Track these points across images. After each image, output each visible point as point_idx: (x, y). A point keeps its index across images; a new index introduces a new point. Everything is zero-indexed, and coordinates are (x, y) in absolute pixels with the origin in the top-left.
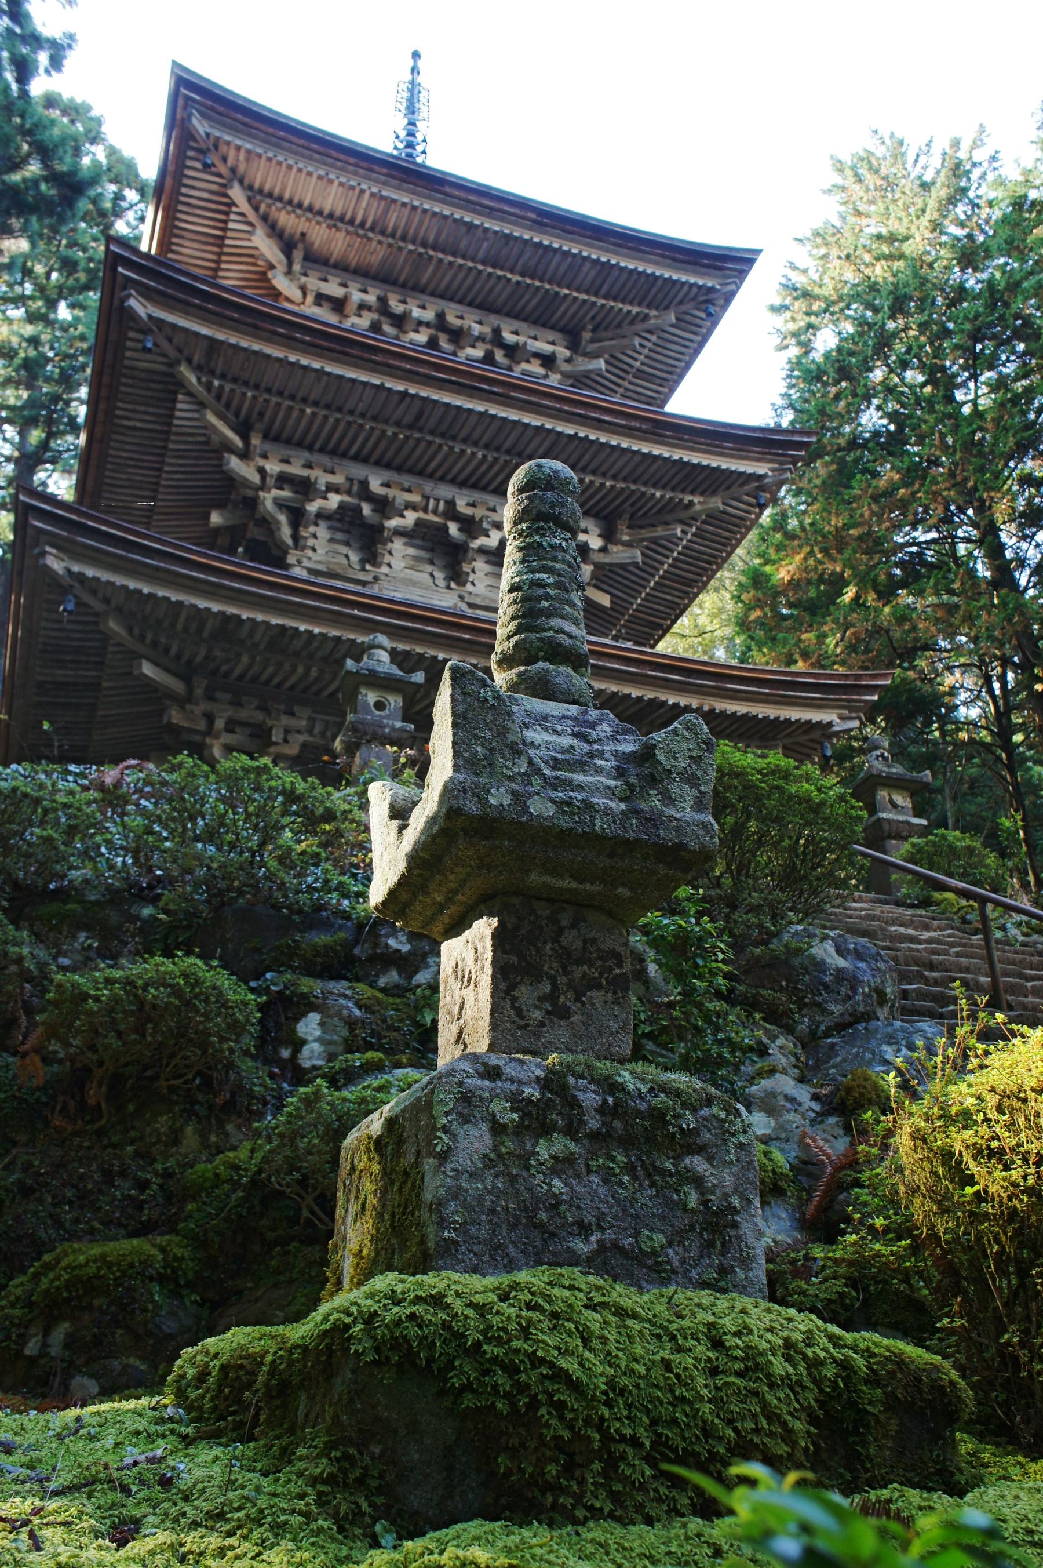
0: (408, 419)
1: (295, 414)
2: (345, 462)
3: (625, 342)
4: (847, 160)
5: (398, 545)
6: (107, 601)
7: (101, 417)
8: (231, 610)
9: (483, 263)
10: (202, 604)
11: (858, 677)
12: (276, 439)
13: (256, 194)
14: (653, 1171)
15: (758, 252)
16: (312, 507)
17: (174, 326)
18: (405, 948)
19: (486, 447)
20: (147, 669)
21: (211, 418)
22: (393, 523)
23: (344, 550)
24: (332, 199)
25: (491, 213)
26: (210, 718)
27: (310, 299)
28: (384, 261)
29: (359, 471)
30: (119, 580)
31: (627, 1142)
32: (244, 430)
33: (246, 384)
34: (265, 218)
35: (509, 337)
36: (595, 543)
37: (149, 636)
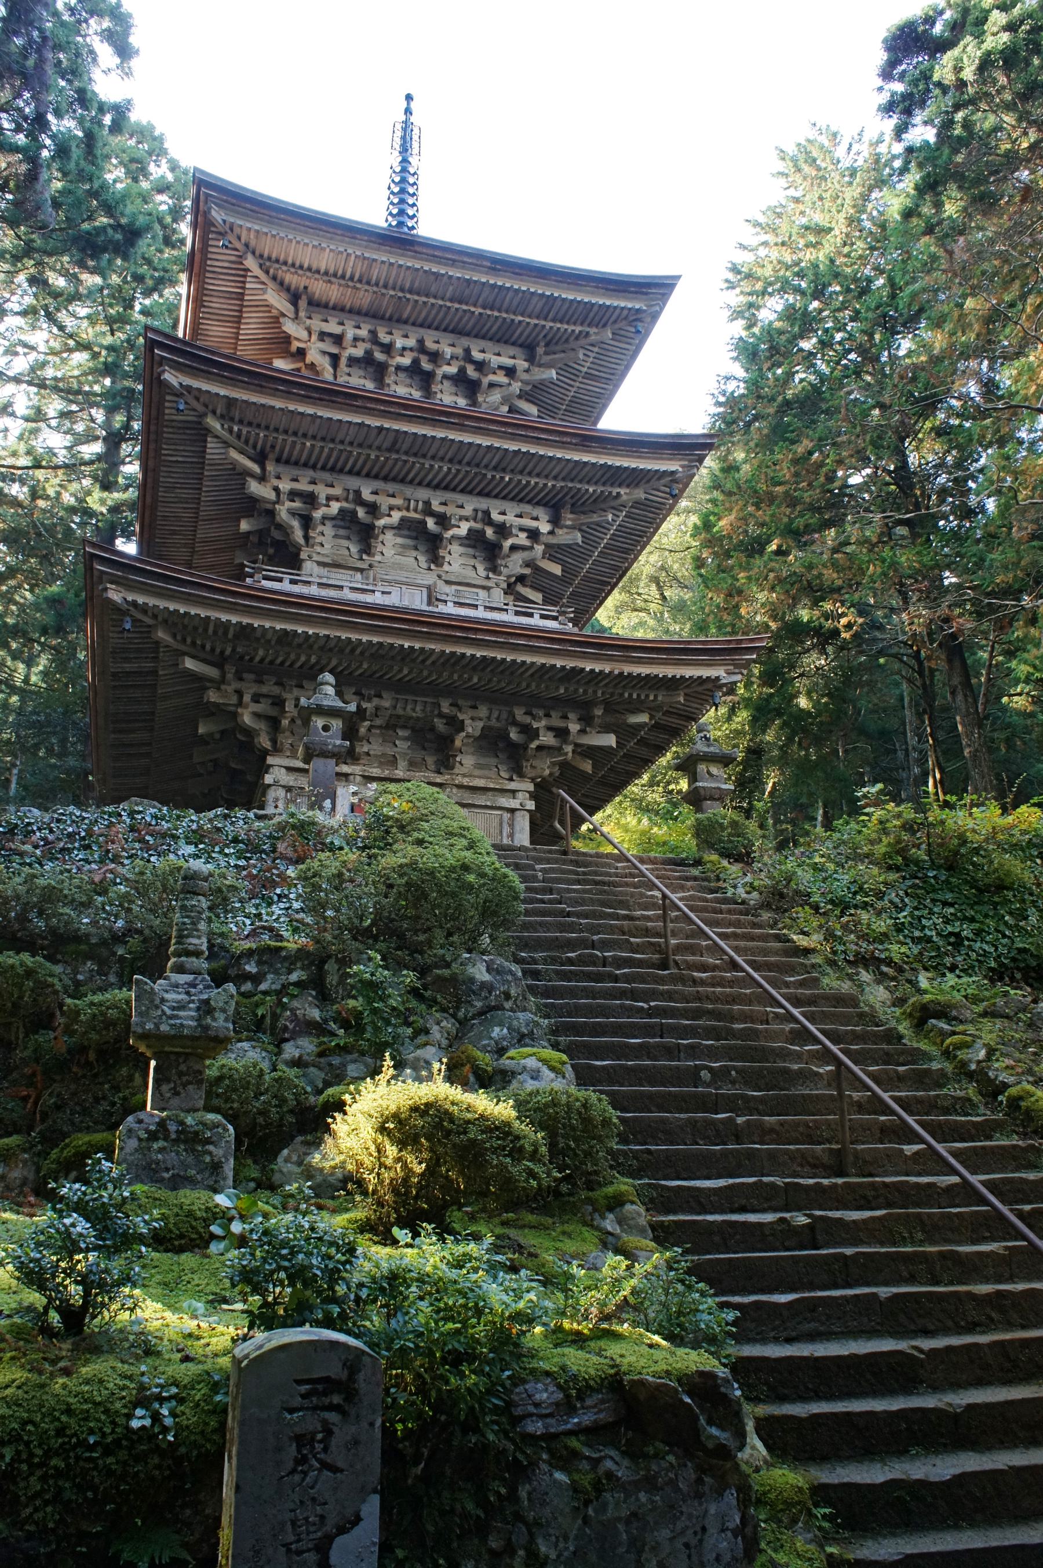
0: (386, 445)
1: (298, 447)
2: (342, 477)
3: (572, 354)
4: (791, 150)
5: (389, 537)
6: (155, 617)
7: (152, 454)
8: (246, 621)
9: (451, 300)
10: (224, 617)
11: (740, 641)
12: (287, 462)
13: (266, 262)
14: (193, 1150)
15: (678, 277)
16: (317, 514)
17: (199, 390)
18: (254, 970)
19: (451, 461)
20: (189, 664)
21: (234, 454)
22: (381, 522)
23: (345, 543)
24: (325, 261)
25: (453, 263)
26: (240, 694)
27: (314, 338)
28: (372, 303)
29: (353, 483)
30: (162, 604)
31: (185, 1142)
32: (260, 459)
33: (259, 426)
34: (274, 278)
35: (477, 355)
36: (545, 528)
37: (189, 640)
